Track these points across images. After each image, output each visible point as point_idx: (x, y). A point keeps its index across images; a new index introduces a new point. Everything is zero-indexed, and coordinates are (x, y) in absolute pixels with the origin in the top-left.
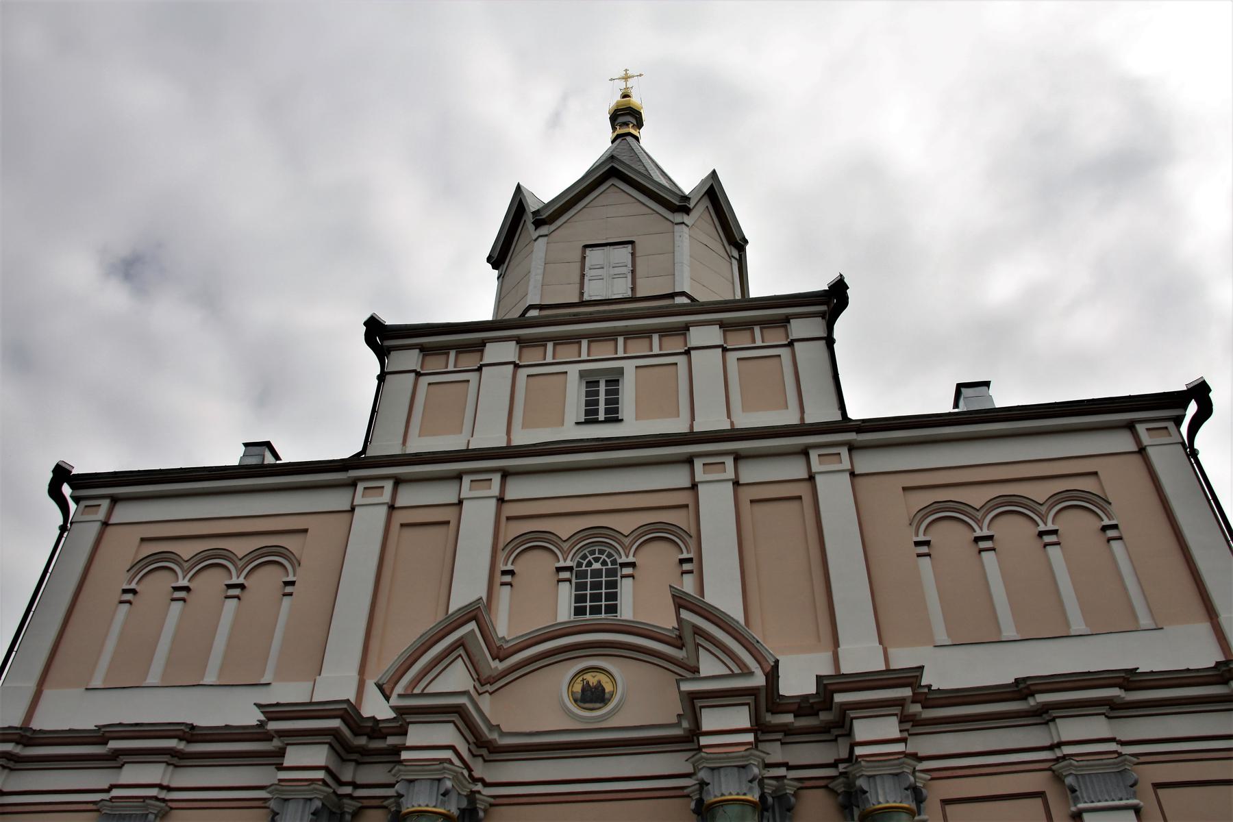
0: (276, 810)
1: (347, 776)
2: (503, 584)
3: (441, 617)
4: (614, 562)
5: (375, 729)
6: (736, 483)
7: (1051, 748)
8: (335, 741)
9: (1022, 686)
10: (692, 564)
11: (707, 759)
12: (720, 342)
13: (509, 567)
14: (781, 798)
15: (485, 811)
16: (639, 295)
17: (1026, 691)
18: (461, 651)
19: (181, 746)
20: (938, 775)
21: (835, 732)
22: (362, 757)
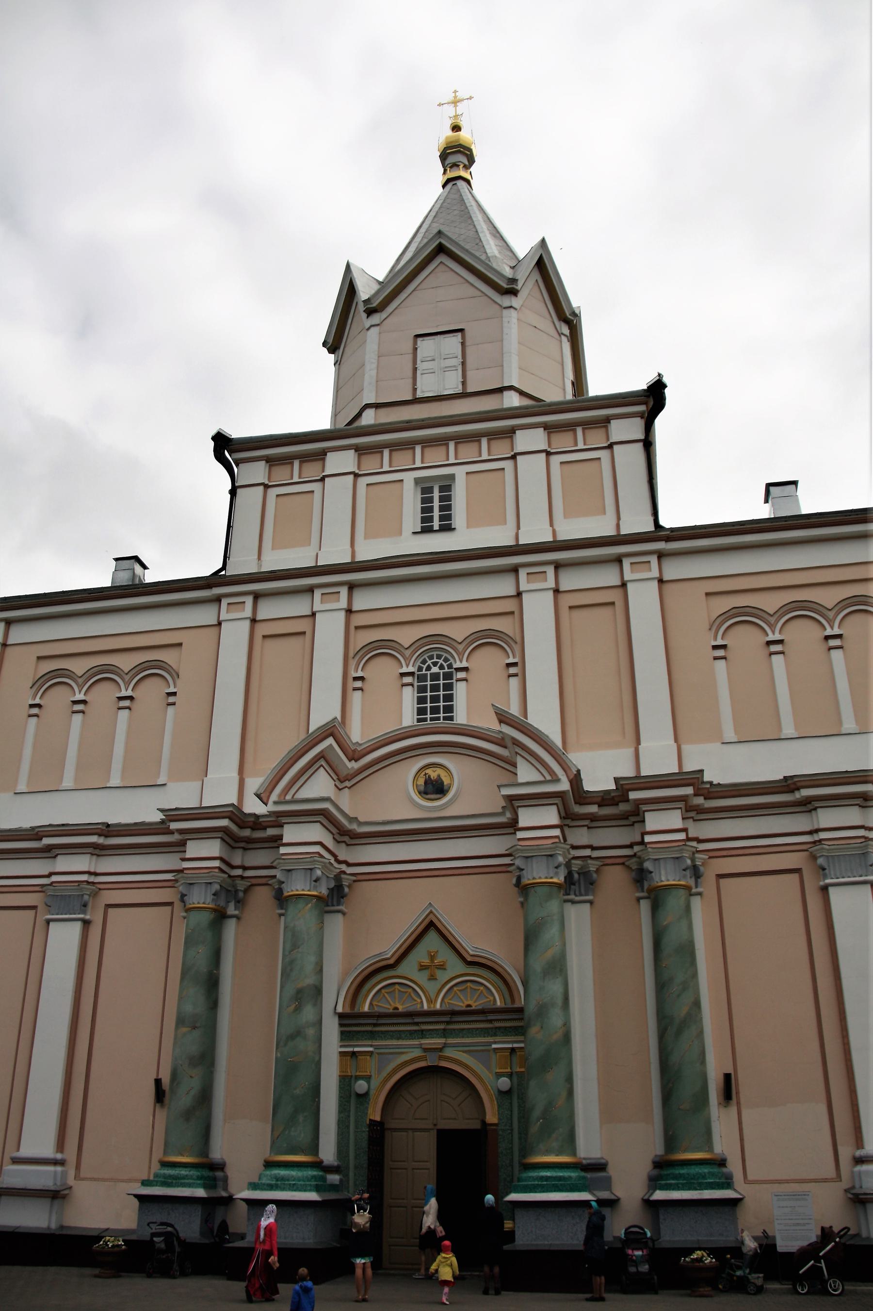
0: (184, 892)
1: (237, 860)
2: (355, 689)
3: (303, 736)
4: (450, 666)
5: (256, 823)
6: (556, 591)
7: (810, 833)
9: (789, 782)
10: (516, 669)
11: (522, 851)
12: (544, 446)
13: (360, 674)
14: (585, 874)
15: (349, 886)
16: (470, 389)
17: (793, 786)
18: (323, 762)
19: (101, 840)
20: (714, 854)
21: (632, 819)
22: (248, 844)
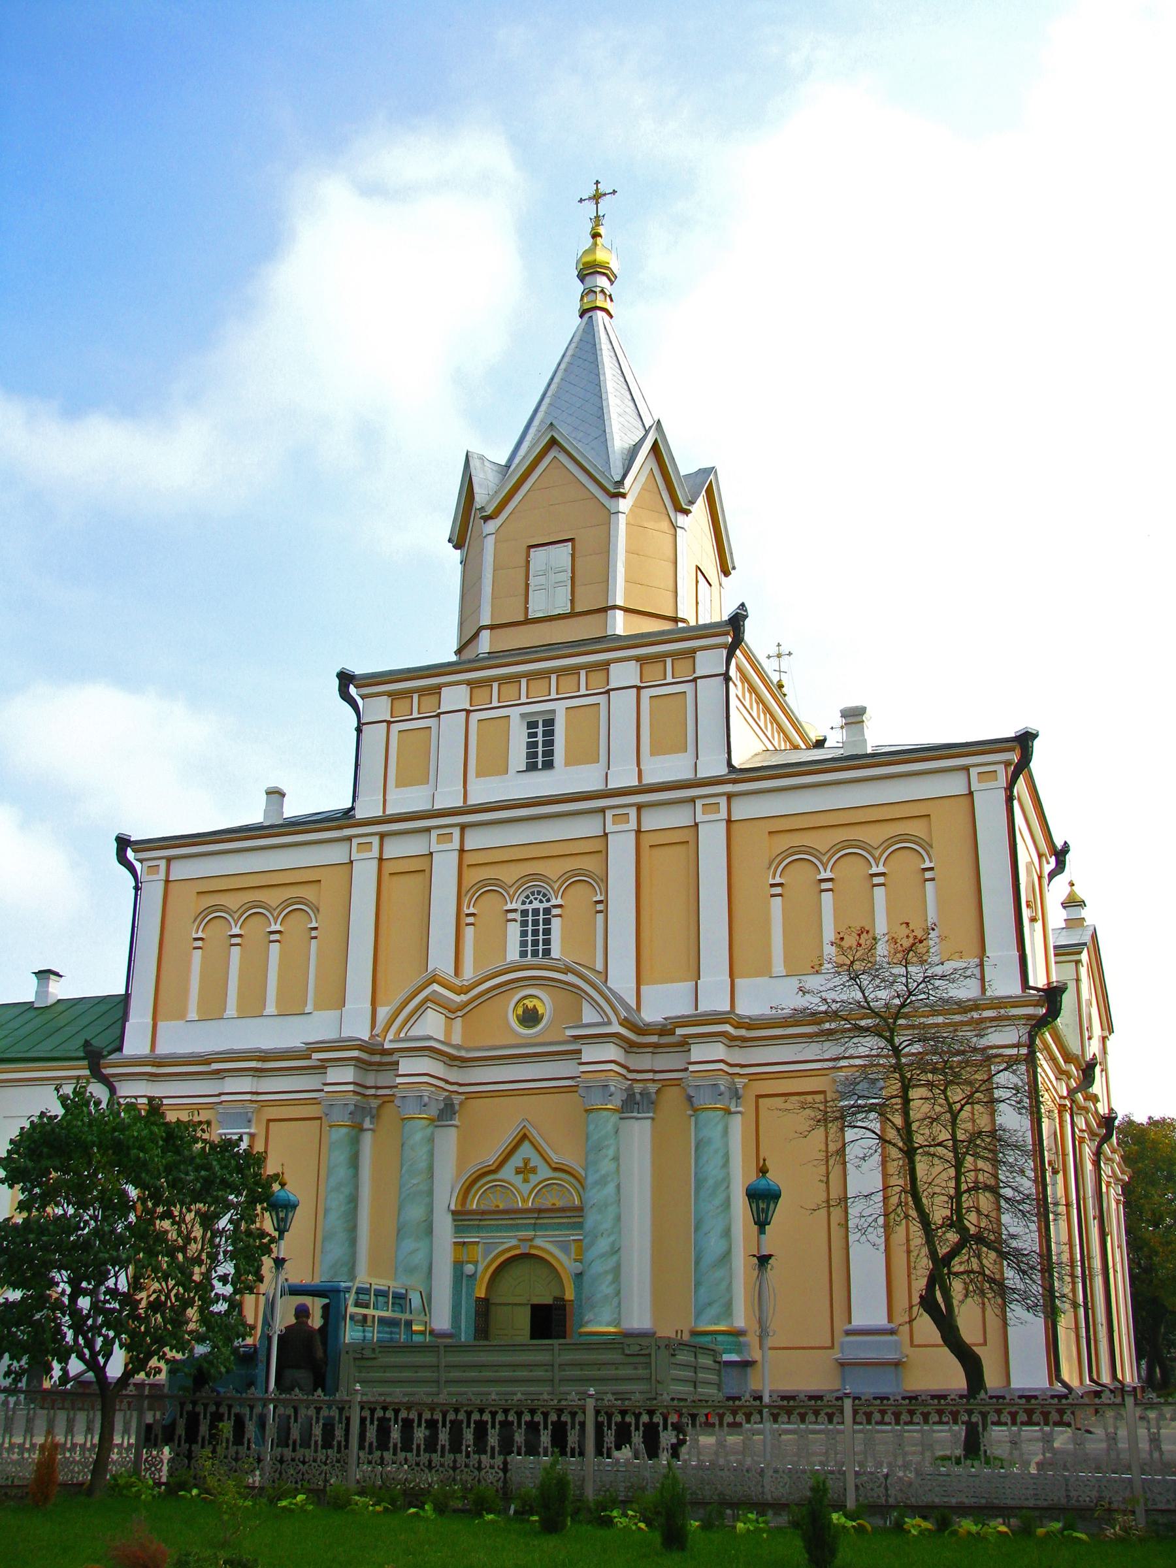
1: (370, 1082)
2: (468, 924)
8: (359, 1063)
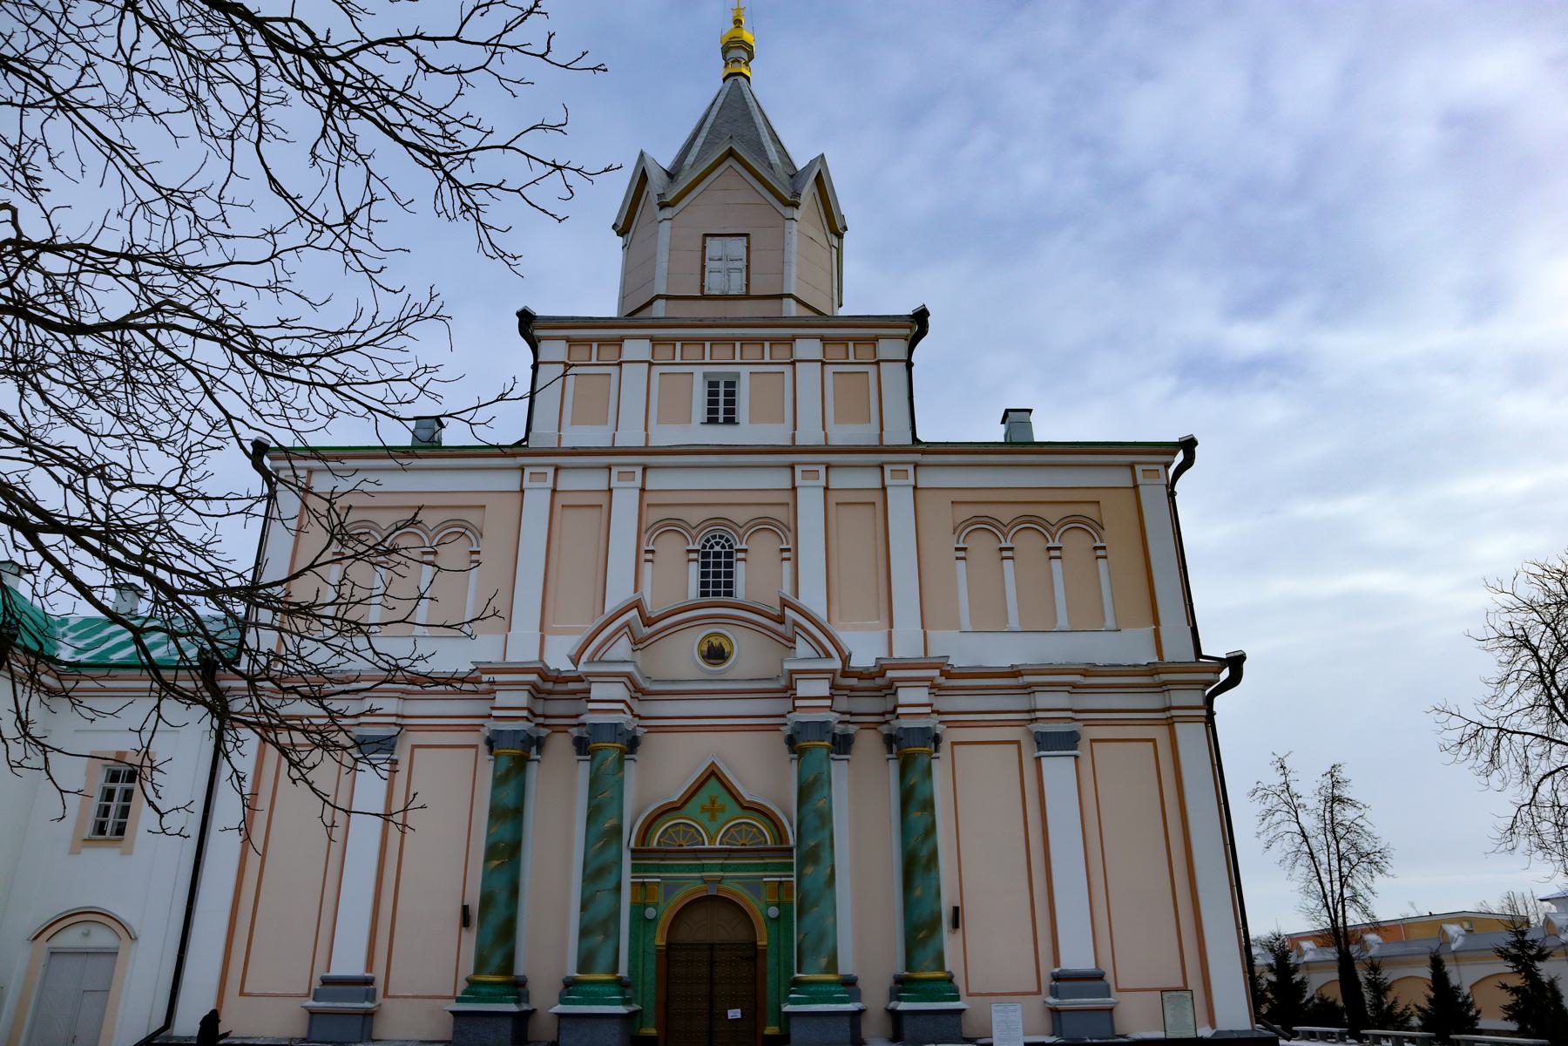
1: (538, 711)
